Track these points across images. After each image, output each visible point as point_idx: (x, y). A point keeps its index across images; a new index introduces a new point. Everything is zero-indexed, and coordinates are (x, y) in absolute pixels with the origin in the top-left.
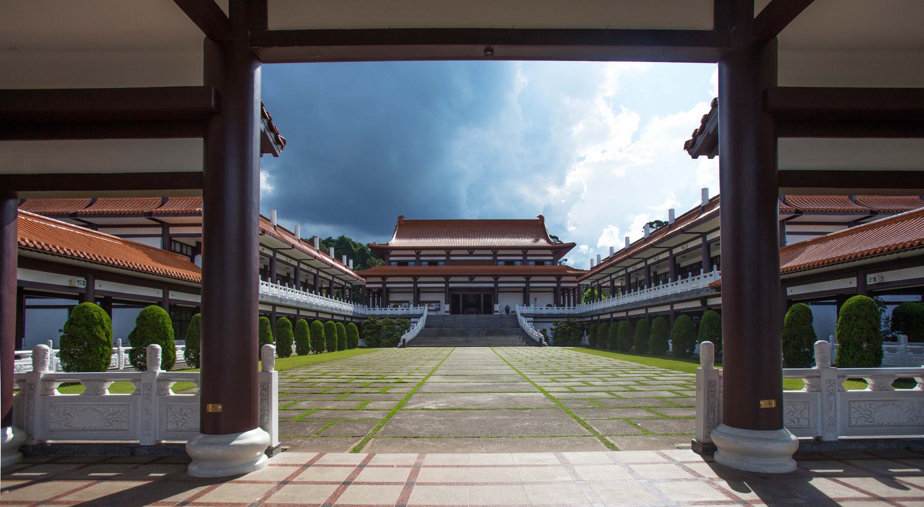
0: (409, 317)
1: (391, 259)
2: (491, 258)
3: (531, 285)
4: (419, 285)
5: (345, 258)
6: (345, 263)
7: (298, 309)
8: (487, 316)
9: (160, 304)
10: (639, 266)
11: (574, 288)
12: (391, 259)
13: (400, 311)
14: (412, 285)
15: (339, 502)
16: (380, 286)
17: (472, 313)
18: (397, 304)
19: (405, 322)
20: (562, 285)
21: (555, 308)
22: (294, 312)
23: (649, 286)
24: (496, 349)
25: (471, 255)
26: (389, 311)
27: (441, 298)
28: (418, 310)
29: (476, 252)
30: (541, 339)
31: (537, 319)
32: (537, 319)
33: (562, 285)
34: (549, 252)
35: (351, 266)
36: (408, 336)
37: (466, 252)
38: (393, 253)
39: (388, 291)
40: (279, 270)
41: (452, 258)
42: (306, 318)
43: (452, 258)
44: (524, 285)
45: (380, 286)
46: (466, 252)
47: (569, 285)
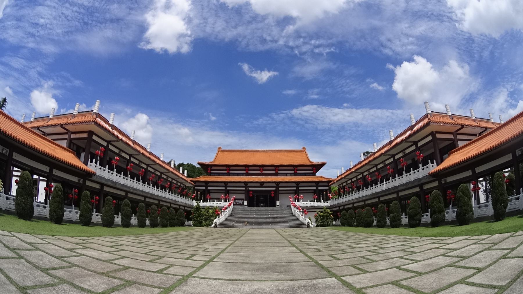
0: (221, 208)
3: (300, 188)
4: (228, 188)
5: (83, 155)
6: (181, 172)
7: (171, 203)
8: (272, 208)
9: (143, 202)
10: (359, 177)
11: (326, 190)
13: (215, 204)
14: (224, 188)
15: (364, 291)
16: (204, 188)
17: (262, 206)
18: (212, 199)
19: (217, 212)
20: (320, 188)
21: (316, 202)
22: (178, 207)
23: (363, 189)
24: (281, 231)
26: (208, 204)
27: (243, 196)
28: (223, 204)
29: (265, 168)
30: (308, 222)
31: (304, 210)
32: (304, 210)
33: (320, 188)
34: (310, 168)
35: (186, 174)
36: (217, 221)
39: (209, 192)
40: (150, 177)
42: (174, 208)
44: (295, 188)
46: (258, 168)
47: (321, 190)
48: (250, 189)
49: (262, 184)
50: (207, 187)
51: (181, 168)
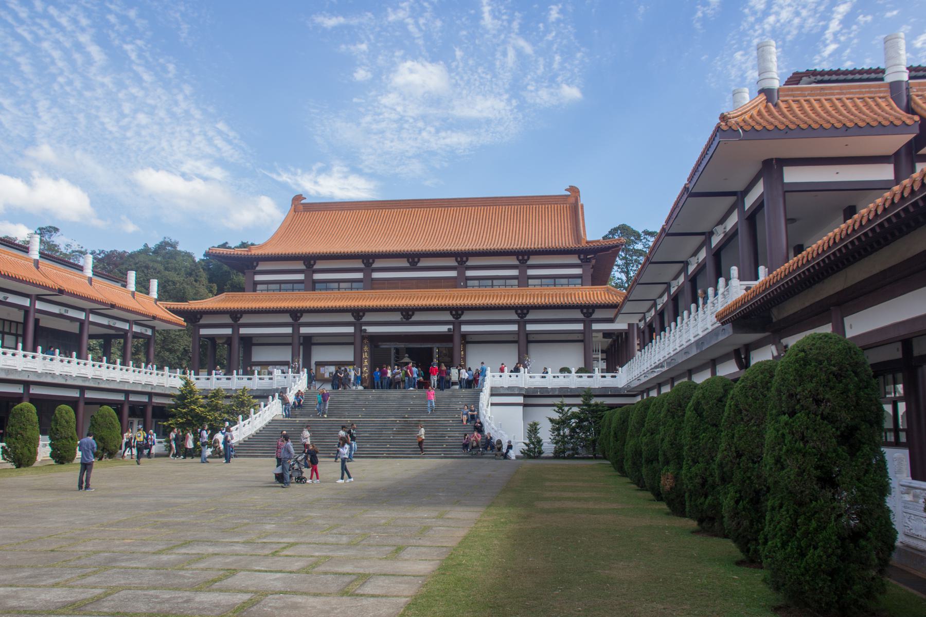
1: (258, 278)
2: (453, 274)
12: (258, 278)
16: (228, 331)
25: (413, 267)
29: (423, 263)
34: (574, 260)
41: (376, 275)
43: (376, 275)
45: (228, 331)
48: (371, 329)
49: (407, 313)
50: (236, 326)
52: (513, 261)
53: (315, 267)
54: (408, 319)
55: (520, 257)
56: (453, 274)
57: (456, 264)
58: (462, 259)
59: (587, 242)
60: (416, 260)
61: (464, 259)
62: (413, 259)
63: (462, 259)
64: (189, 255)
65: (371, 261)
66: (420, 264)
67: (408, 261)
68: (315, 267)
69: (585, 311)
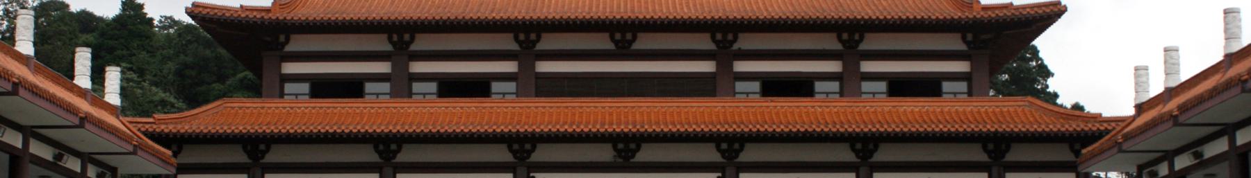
2: (707, 67)
6: (83, 80)
10: (1211, 150)
12: (290, 68)
25: (623, 52)
29: (645, 42)
34: (953, 42)
35: (113, 96)
37: (601, 42)
38: (298, 44)
41: (545, 67)
43: (545, 67)
51: (83, 59)
52: (380, 43)
53: (413, 47)
54: (627, 159)
55: (618, 36)
56: (707, 67)
57: (839, 47)
58: (725, 36)
59: (986, 8)
60: (407, 37)
61: (407, 37)
62: (623, 34)
63: (623, 36)
64: (171, 22)
65: (282, 38)
66: (637, 46)
67: (390, 40)
68: (413, 47)
69: (724, 146)
